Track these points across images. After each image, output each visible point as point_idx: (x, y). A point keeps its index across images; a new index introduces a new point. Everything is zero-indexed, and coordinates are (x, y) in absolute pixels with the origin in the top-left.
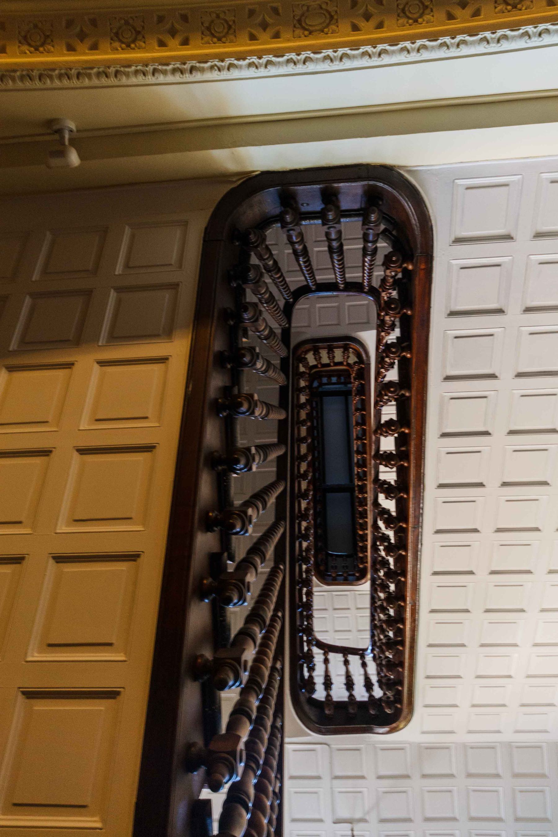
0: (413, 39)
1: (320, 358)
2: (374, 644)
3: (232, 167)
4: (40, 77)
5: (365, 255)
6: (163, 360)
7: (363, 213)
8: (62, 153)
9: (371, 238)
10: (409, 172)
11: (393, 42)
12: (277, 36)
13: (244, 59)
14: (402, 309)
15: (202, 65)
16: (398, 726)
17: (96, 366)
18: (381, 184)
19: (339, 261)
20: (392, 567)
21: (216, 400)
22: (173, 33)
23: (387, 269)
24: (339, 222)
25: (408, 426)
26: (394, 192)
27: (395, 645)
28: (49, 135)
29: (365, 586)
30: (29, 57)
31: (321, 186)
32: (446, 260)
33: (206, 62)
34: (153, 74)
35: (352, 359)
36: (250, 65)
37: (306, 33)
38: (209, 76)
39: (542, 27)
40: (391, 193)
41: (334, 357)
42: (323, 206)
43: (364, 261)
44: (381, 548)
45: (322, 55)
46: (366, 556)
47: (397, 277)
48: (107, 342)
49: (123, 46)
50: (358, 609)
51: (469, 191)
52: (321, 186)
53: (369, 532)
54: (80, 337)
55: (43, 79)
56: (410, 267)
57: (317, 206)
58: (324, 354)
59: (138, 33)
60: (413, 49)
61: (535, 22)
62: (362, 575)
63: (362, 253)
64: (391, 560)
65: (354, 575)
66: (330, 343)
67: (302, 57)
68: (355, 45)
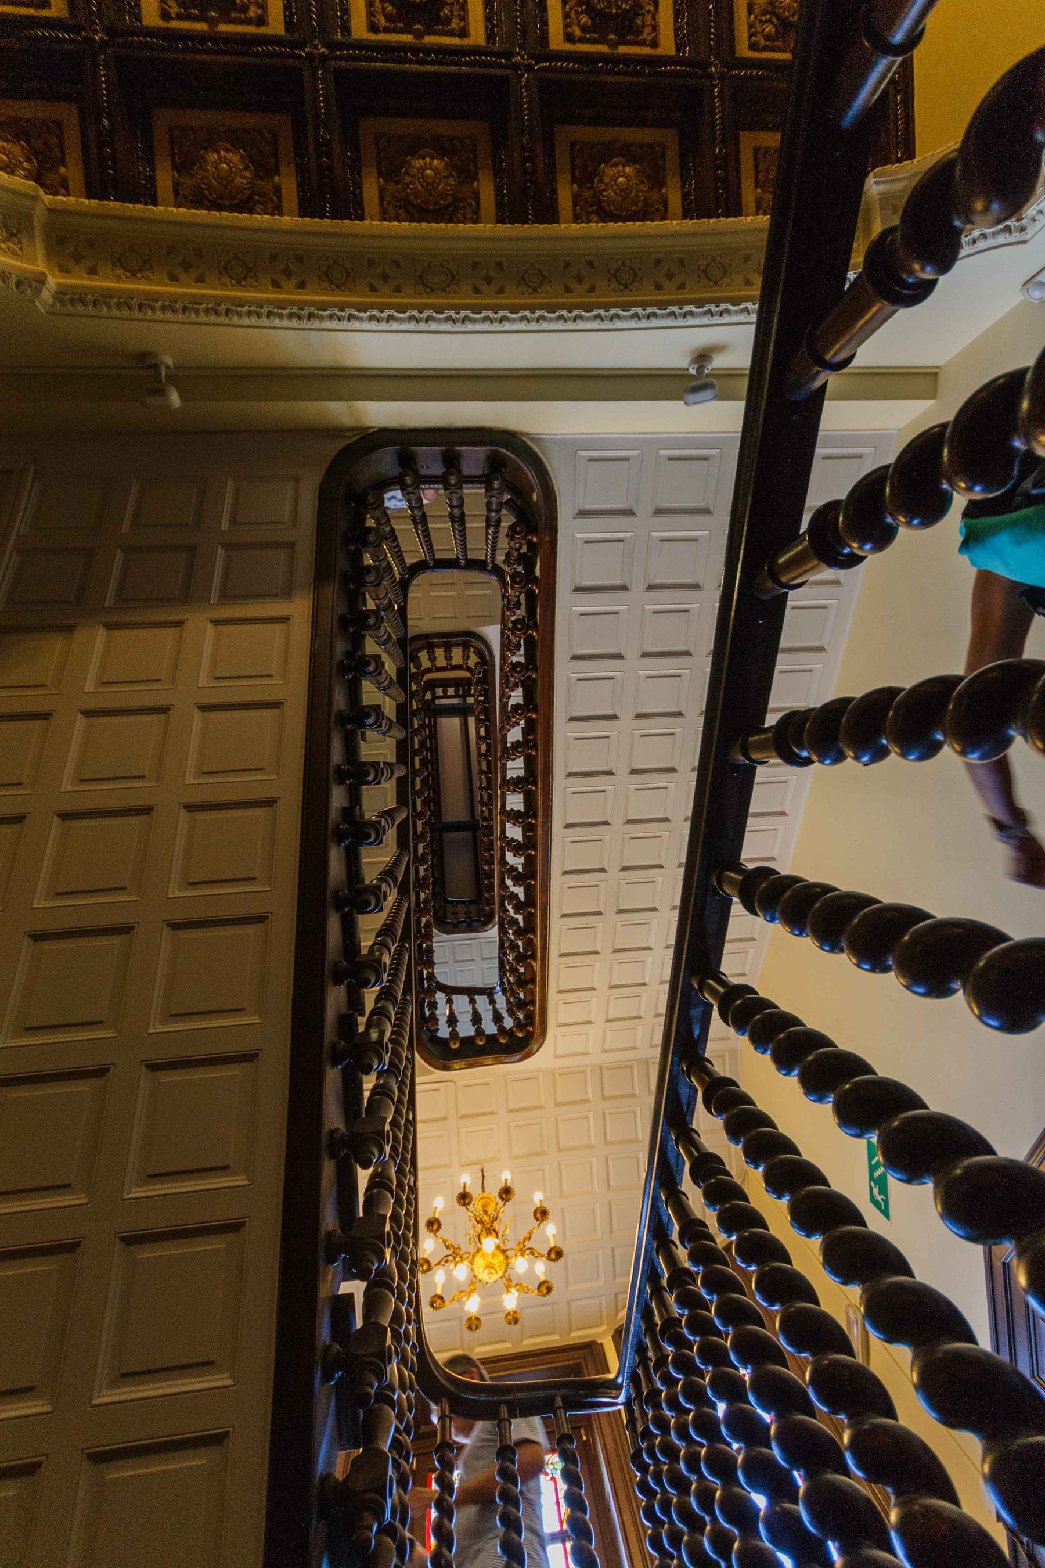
0: (533, 309)
1: (435, 658)
2: (502, 984)
3: (348, 421)
4: (140, 307)
5: (488, 526)
6: (285, 619)
7: (485, 480)
8: (162, 392)
9: (494, 507)
10: (532, 439)
11: (514, 309)
12: (398, 290)
13: (366, 311)
14: (527, 583)
15: (321, 313)
16: (531, 1050)
17: (210, 625)
18: (504, 451)
19: (460, 531)
20: (521, 950)
21: (342, 662)
22: (288, 274)
23: (512, 540)
24: (461, 488)
25: (535, 710)
26: (519, 461)
27: (526, 981)
28: (143, 372)
29: (493, 933)
30: (124, 282)
31: (443, 448)
32: (571, 534)
33: (325, 310)
34: (268, 317)
35: (473, 660)
36: (371, 318)
37: (428, 290)
38: (327, 324)
39: (650, 310)
40: (516, 462)
41: (451, 658)
42: (444, 470)
43: (487, 534)
44: (511, 932)
45: (445, 315)
46: (493, 896)
47: (521, 551)
48: (219, 600)
49: (234, 282)
50: (484, 959)
51: (592, 463)
52: (443, 448)
53: (496, 867)
54: (188, 594)
55: (22, 289)
56: (535, 540)
57: (438, 469)
58: (440, 652)
59: (249, 269)
60: (533, 319)
61: (644, 305)
62: (489, 919)
63: (482, 526)
64: (520, 943)
65: (479, 920)
66: (447, 640)
67: (425, 315)
68: (477, 309)
